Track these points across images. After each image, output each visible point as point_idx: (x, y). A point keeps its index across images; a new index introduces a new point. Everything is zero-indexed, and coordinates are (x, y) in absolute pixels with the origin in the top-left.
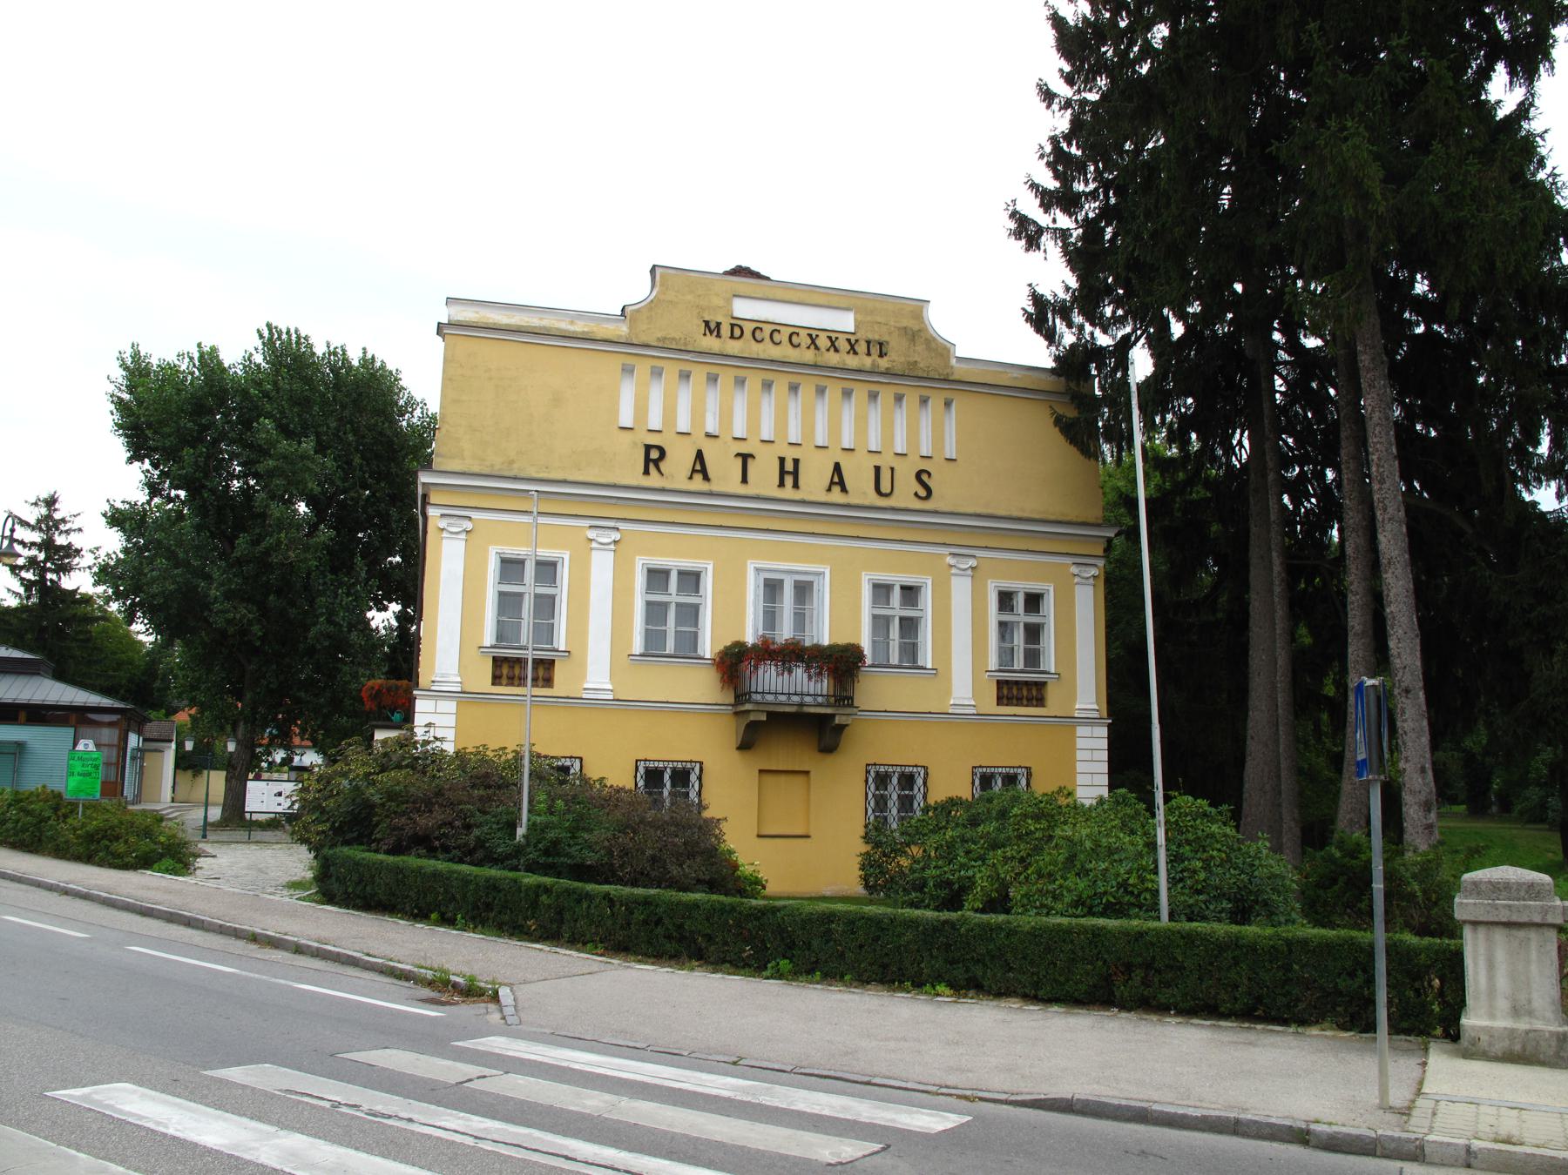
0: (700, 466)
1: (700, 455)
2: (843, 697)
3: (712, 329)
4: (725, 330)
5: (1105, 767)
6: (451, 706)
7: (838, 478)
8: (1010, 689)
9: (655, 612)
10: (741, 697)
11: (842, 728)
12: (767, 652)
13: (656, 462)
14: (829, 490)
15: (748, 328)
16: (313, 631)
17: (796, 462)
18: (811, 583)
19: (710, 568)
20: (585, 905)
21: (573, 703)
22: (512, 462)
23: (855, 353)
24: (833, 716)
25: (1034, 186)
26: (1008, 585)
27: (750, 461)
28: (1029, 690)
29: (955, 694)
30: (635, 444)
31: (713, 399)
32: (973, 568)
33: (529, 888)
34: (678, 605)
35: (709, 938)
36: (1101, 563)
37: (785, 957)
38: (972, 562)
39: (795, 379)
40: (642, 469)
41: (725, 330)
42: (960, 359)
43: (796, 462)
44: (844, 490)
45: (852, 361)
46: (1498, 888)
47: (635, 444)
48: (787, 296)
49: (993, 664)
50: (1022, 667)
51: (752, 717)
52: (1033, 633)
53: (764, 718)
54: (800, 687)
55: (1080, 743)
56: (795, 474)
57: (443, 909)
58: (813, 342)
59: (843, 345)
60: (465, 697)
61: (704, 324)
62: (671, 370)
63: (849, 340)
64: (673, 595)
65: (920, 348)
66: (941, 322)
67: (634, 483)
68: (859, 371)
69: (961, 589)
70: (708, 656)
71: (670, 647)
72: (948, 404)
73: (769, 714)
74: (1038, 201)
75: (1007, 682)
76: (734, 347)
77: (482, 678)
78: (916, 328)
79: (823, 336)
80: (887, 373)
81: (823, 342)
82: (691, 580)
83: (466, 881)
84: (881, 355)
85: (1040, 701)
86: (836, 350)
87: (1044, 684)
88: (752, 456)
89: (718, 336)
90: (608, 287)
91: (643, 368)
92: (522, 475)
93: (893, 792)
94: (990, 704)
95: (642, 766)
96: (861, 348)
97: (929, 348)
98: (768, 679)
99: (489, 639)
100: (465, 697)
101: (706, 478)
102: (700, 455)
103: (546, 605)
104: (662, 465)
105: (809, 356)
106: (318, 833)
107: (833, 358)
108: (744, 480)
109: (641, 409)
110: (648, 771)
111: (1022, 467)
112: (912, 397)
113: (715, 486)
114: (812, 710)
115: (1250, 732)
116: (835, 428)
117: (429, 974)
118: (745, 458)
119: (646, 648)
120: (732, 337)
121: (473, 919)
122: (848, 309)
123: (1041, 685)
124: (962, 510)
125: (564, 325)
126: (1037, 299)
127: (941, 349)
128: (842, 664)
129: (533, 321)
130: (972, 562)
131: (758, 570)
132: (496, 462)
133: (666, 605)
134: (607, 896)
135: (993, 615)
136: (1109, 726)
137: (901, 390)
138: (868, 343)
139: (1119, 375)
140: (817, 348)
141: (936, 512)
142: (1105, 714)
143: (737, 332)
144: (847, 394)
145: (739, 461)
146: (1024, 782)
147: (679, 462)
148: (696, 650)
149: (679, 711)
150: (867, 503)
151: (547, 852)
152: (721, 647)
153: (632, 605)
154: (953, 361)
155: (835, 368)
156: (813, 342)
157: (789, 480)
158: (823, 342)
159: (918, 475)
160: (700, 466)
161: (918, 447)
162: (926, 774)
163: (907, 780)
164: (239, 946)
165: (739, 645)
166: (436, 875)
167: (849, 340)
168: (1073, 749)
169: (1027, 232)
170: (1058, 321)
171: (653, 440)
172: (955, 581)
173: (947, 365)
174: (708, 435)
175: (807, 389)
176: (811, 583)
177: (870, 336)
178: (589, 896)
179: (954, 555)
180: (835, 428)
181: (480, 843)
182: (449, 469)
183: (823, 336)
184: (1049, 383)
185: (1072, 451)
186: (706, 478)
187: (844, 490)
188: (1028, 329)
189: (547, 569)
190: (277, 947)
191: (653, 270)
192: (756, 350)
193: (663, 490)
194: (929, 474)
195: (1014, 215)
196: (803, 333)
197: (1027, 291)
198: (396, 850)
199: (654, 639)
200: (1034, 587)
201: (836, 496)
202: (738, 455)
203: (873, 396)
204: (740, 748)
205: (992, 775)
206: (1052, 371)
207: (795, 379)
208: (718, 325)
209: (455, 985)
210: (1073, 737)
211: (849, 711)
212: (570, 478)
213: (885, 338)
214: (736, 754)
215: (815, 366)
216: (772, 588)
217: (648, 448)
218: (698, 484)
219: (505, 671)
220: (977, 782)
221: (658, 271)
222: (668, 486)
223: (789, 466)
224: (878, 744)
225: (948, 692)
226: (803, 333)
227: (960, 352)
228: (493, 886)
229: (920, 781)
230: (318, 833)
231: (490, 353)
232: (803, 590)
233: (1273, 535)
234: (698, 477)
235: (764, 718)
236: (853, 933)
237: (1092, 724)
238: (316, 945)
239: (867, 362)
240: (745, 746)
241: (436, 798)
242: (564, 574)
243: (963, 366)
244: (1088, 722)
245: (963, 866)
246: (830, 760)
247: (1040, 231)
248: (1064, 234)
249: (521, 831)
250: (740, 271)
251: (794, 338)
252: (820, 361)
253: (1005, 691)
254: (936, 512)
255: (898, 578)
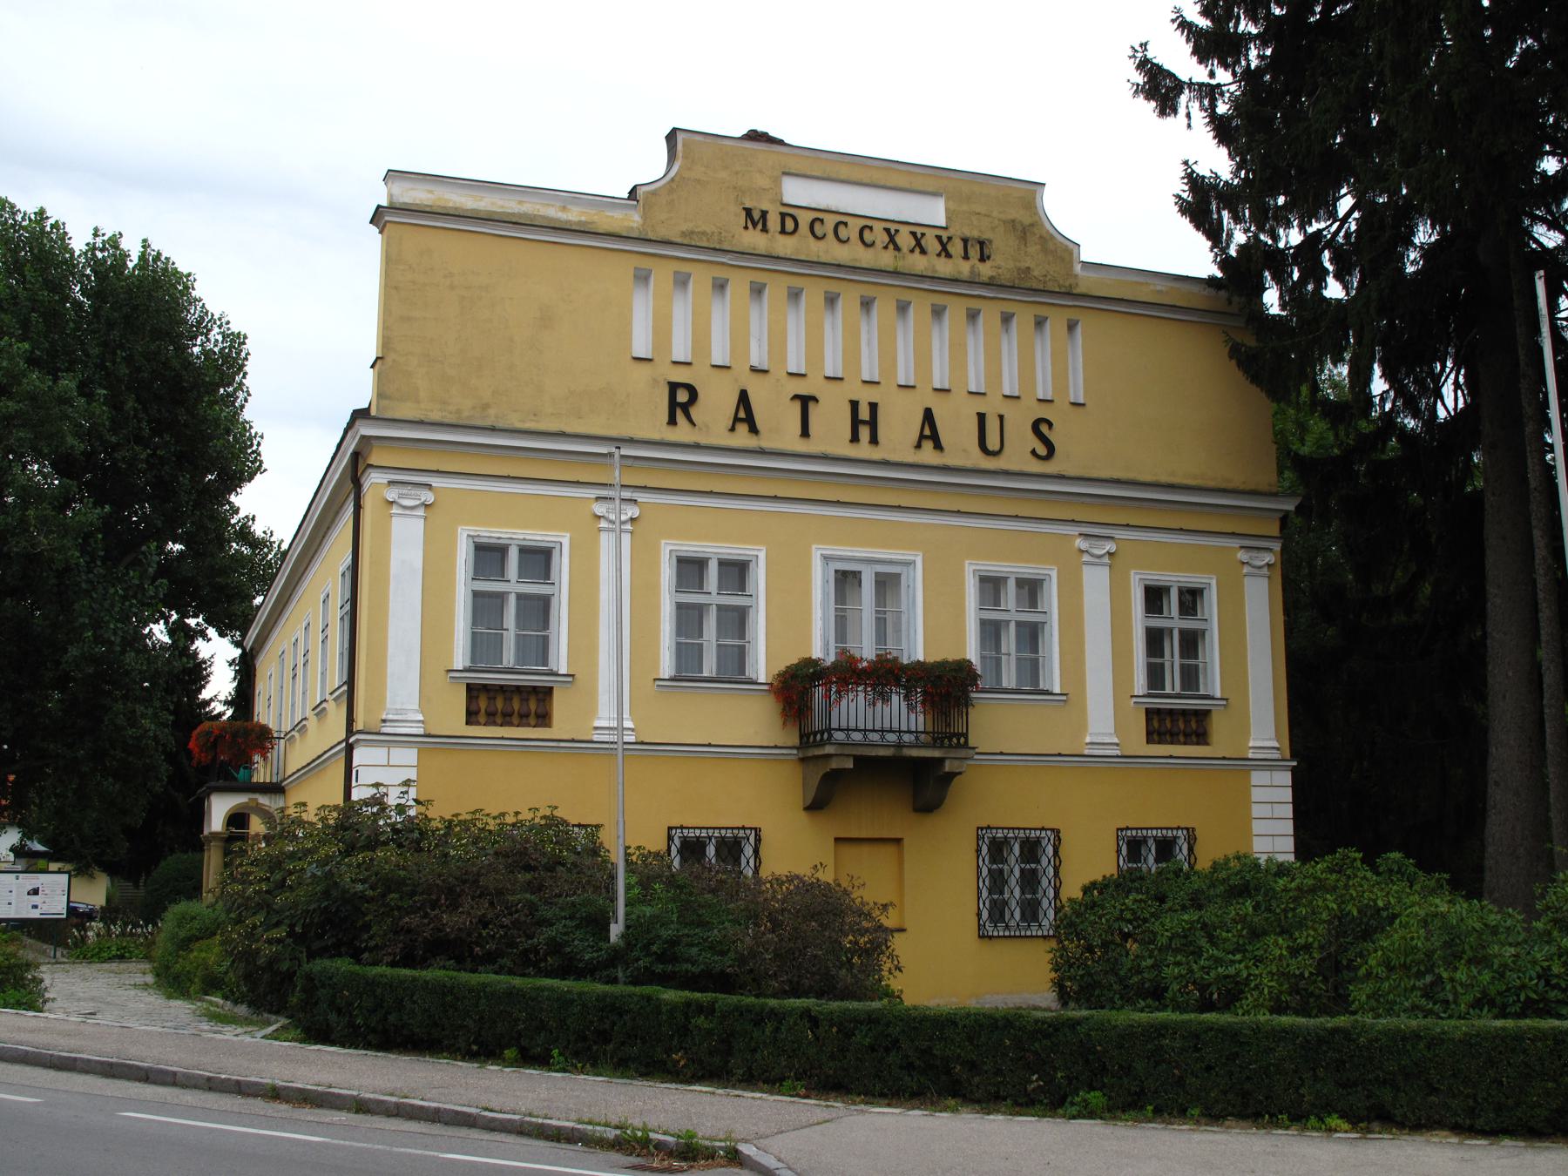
0: (744, 412)
1: (744, 398)
2: (950, 735)
3: (755, 219)
4: (774, 222)
5: (1289, 827)
6: (409, 756)
7: (930, 430)
9: (689, 618)
11: (952, 776)
12: (847, 673)
13: (685, 408)
15: (805, 219)
16: (73, 651)
17: (873, 407)
18: (898, 576)
19: (762, 555)
20: (769, 1029)
21: (581, 747)
22: (486, 407)
23: (949, 256)
24: (941, 761)
25: (1184, 25)
26: (1159, 577)
27: (811, 405)
28: (1187, 722)
29: (1090, 730)
30: (655, 381)
32: (1110, 554)
33: (673, 1008)
34: (520, 597)
35: (973, 1066)
36: (1277, 546)
38: (1110, 546)
39: (869, 292)
40: (666, 418)
41: (774, 222)
42: (1088, 265)
43: (873, 407)
44: (938, 446)
45: (944, 267)
46: (211, 1003)
47: (655, 381)
49: (1132, 682)
50: (1178, 689)
52: (1191, 642)
53: (850, 764)
55: (1257, 794)
56: (873, 423)
58: (918, 243)
59: (932, 245)
60: (429, 743)
61: (734, 207)
62: (701, 278)
63: (939, 238)
64: (513, 583)
65: (1033, 249)
66: (1063, 213)
67: (656, 436)
68: (955, 281)
69: (1096, 583)
70: (762, 679)
71: (709, 667)
72: (1071, 327)
73: (858, 760)
74: (1189, 48)
75: (1158, 711)
76: (785, 245)
77: (452, 717)
78: (1027, 221)
80: (990, 284)
81: (905, 240)
82: (736, 572)
83: (564, 1001)
84: (982, 259)
85: (1201, 737)
86: (923, 252)
87: (1207, 713)
88: (815, 399)
89: (765, 230)
90: (614, 162)
91: (662, 274)
92: (500, 425)
93: (1014, 868)
95: (677, 834)
96: (956, 248)
97: (1045, 250)
98: (854, 711)
99: (460, 660)
101: (754, 430)
102: (744, 398)
103: (538, 611)
104: (693, 412)
105: (886, 259)
107: (918, 263)
108: (805, 433)
109: (662, 333)
110: (685, 842)
111: (1177, 419)
113: (765, 442)
114: (915, 753)
115: (1493, 777)
116: (923, 359)
117: (611, 1134)
118: (805, 401)
119: (473, 660)
120: (783, 231)
121: (576, 1054)
123: (544, 694)
124: (1095, 474)
126: (1193, 180)
127: (1062, 250)
128: (946, 688)
129: (510, 205)
132: (462, 406)
133: (502, 597)
135: (1139, 621)
136: (1294, 771)
137: (1009, 308)
138: (965, 241)
139: (1310, 287)
140: (897, 248)
141: (1061, 477)
142: (1288, 755)
143: (790, 225)
144: (938, 312)
145: (797, 405)
146: (1050, 850)
147: (716, 406)
148: (742, 670)
150: (969, 464)
151: (661, 958)
152: (781, 666)
154: (1078, 268)
155: (922, 277)
156: (918, 243)
157: (864, 433)
158: (905, 240)
159: (1036, 426)
160: (744, 412)
161: (784, 360)
162: (758, 840)
163: (1031, 849)
164: (258, 1105)
165: (809, 662)
166: (511, 994)
167: (939, 238)
168: (1246, 802)
169: (1160, 88)
170: (1225, 214)
171: (680, 376)
172: (606, 542)
173: (1070, 273)
174: (754, 370)
176: (898, 576)
177: (967, 233)
178: (777, 1016)
180: (923, 359)
181: (555, 947)
182: (397, 416)
183: (904, 230)
184: (1200, 299)
185: (1256, 394)
186: (754, 430)
187: (938, 446)
188: (1185, 224)
189: (538, 560)
190: (320, 1106)
191: (672, 137)
192: (816, 250)
193: (697, 447)
194: (1050, 425)
195: (1146, 65)
197: (1180, 171)
199: (688, 655)
200: (1192, 579)
201: (928, 455)
202: (796, 397)
205: (1145, 840)
207: (869, 292)
208: (764, 214)
209: (660, 1146)
210: (1246, 788)
211: (962, 753)
212: (568, 430)
213: (986, 236)
215: (895, 273)
216: (846, 580)
217: (674, 387)
218: (742, 438)
219: (483, 704)
220: (985, 849)
221: (680, 137)
222: (703, 441)
223: (864, 414)
224: (994, 799)
225: (1082, 727)
227: (1086, 256)
228: (612, 1007)
229: (748, 851)
230: (270, 942)
232: (887, 584)
233: (1533, 507)
234: (743, 429)
235: (850, 764)
236: (1197, 1050)
237: (1271, 768)
239: (964, 268)
240: (816, 805)
242: (563, 566)
243: (1092, 275)
244: (1267, 765)
247: (1178, 86)
248: (1209, 92)
249: (616, 930)
250: (755, 136)
251: (867, 234)
252: (902, 265)
253: (1156, 724)
254: (1061, 477)
255: (1175, 578)
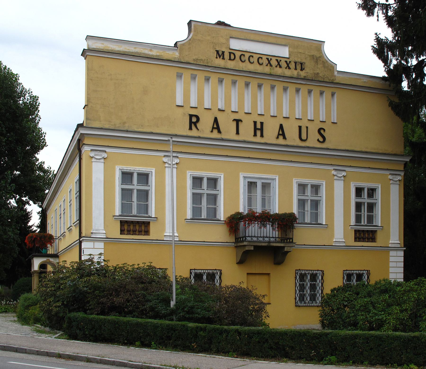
0: (216, 125)
2: (286, 238)
3: (220, 55)
4: (227, 55)
5: (402, 270)
8: (360, 234)
10: (238, 240)
11: (287, 252)
12: (251, 217)
13: (195, 124)
14: (278, 138)
15: (238, 54)
17: (262, 123)
18: (270, 183)
19: (222, 176)
21: (160, 243)
22: (124, 123)
23: (289, 68)
24: (284, 247)
26: (361, 184)
27: (240, 123)
29: (335, 237)
31: (221, 91)
32: (344, 176)
33: (192, 329)
34: (208, 194)
35: (292, 348)
36: (402, 174)
37: (332, 355)
38: (344, 174)
40: (188, 127)
41: (227, 55)
43: (262, 123)
44: (285, 138)
45: (288, 73)
48: (257, 38)
50: (366, 223)
51: (247, 248)
52: (371, 207)
54: (269, 233)
55: (391, 259)
57: (142, 340)
58: (269, 62)
59: (284, 65)
60: (108, 241)
62: (201, 76)
63: (286, 62)
65: (320, 66)
66: (331, 53)
67: (185, 134)
68: (291, 78)
70: (222, 219)
71: (204, 215)
72: (333, 95)
73: (255, 247)
76: (231, 64)
77: (116, 232)
78: (318, 55)
79: (274, 59)
81: (274, 62)
82: (213, 182)
83: (156, 327)
84: (302, 70)
86: (280, 67)
87: (375, 231)
88: (241, 121)
89: (223, 58)
90: (170, 33)
92: (130, 129)
93: (308, 283)
94: (351, 242)
95: (193, 272)
96: (292, 66)
97: (324, 67)
98: (254, 230)
99: (118, 212)
100: (108, 241)
103: (144, 195)
104: (198, 125)
105: (267, 70)
106: (56, 307)
107: (278, 71)
108: (238, 133)
109: (187, 96)
111: (369, 128)
112: (316, 91)
114: (275, 245)
118: (238, 122)
119: (122, 212)
120: (230, 59)
121: (160, 344)
122: (285, 45)
123: (374, 232)
124: (339, 148)
125: (147, 52)
126: (379, 41)
127: (330, 66)
128: (286, 222)
130: (344, 174)
131: (245, 177)
132: (116, 123)
133: (131, 190)
134: (237, 331)
138: (296, 63)
139: (419, 80)
140: (271, 66)
141: (327, 149)
142: (403, 246)
143: (232, 57)
144: (285, 89)
145: (235, 123)
147: (206, 123)
148: (147, 213)
149: (209, 246)
150: (295, 144)
151: (188, 312)
152: (229, 215)
153: (186, 194)
154: (336, 73)
155: (280, 76)
156: (269, 62)
157: (259, 133)
158: (274, 62)
160: (216, 125)
162: (221, 274)
163: (314, 277)
165: (239, 213)
167: (286, 62)
168: (388, 262)
170: (390, 53)
174: (219, 110)
175: (266, 87)
176: (270, 183)
178: (227, 332)
179: (92, 150)
180: (280, 107)
181: (152, 309)
182: (93, 126)
183: (274, 59)
185: (398, 119)
190: (75, 360)
191: (190, 23)
193: (199, 138)
194: (324, 130)
196: (264, 58)
197: (374, 37)
198: (103, 313)
199: (196, 211)
201: (281, 141)
202: (234, 120)
203: (234, 83)
204: (237, 263)
206: (384, 78)
207: (261, 81)
208: (223, 52)
211: (291, 245)
213: (303, 61)
214: (236, 266)
215: (270, 75)
216: (251, 185)
217: (191, 116)
218: (215, 134)
219: (126, 227)
220: (298, 277)
221: (193, 23)
222: (201, 136)
223: (259, 126)
224: (302, 260)
225: (332, 236)
226: (264, 58)
228: (172, 329)
229: (217, 277)
230: (56, 307)
231: (112, 66)
232: (266, 186)
236: (367, 343)
237: (397, 250)
238: (99, 358)
239: (295, 73)
240: (240, 262)
241: (118, 289)
242: (153, 180)
243: (341, 75)
244: (395, 249)
245: (376, 314)
246: (280, 267)
249: (173, 303)
250: (220, 23)
253: (358, 235)
254: (327, 149)
255: (366, 185)
